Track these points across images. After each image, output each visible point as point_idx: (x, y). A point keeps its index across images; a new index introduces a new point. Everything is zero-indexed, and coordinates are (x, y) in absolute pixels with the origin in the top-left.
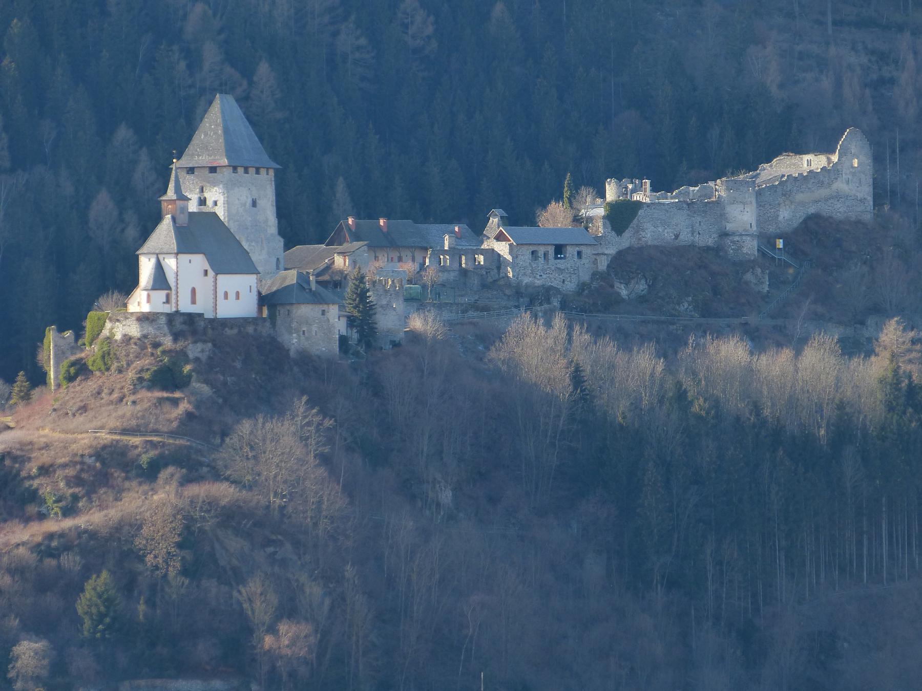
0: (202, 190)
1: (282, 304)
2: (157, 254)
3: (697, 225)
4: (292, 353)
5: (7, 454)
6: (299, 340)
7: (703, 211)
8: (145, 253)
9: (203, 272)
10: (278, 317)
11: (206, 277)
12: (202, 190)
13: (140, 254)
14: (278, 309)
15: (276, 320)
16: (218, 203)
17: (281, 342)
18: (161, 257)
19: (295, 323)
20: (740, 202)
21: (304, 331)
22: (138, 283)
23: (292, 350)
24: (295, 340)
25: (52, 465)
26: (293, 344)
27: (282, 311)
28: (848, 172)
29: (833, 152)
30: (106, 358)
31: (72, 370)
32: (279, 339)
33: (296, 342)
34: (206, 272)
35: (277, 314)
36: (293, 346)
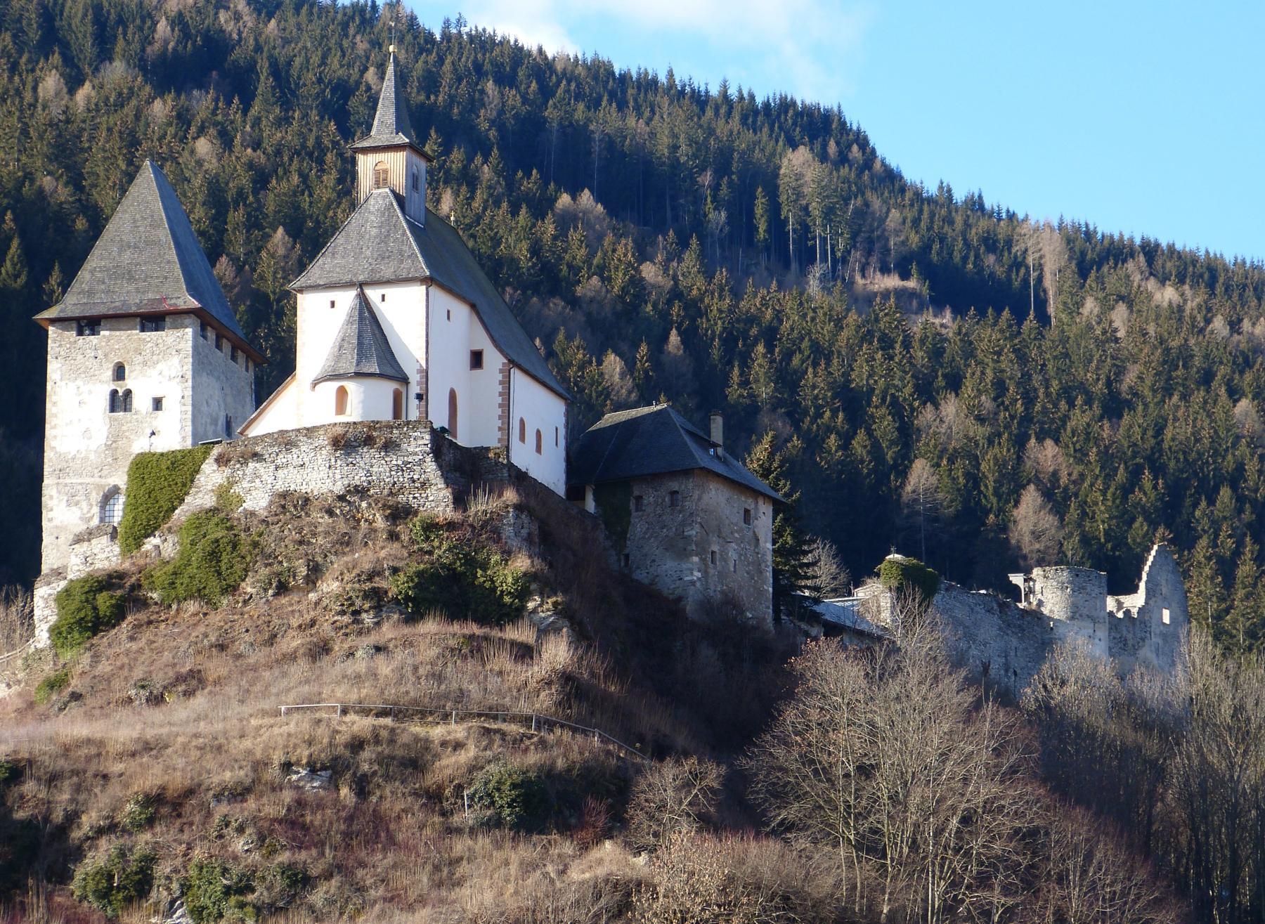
0: (119, 373)
1: (655, 478)
2: (361, 285)
3: (1012, 653)
4: (690, 608)
5: (16, 771)
6: (705, 574)
7: (1020, 626)
8: (320, 285)
9: (466, 359)
10: (634, 514)
11: (478, 372)
12: (119, 373)
13: (301, 290)
14: (636, 493)
15: (629, 523)
16: (164, 402)
17: (646, 581)
18: (373, 294)
19: (697, 527)
20: (1088, 616)
21: (713, 553)
22: (294, 368)
23: (690, 599)
24: (697, 574)
25: (190, 792)
26: (693, 583)
27: (650, 498)
28: (1158, 632)
29: (1133, 589)
30: (225, 558)
31: (104, 601)
32: (641, 576)
33: (699, 579)
34: (477, 359)
35: (632, 506)
36: (691, 590)
